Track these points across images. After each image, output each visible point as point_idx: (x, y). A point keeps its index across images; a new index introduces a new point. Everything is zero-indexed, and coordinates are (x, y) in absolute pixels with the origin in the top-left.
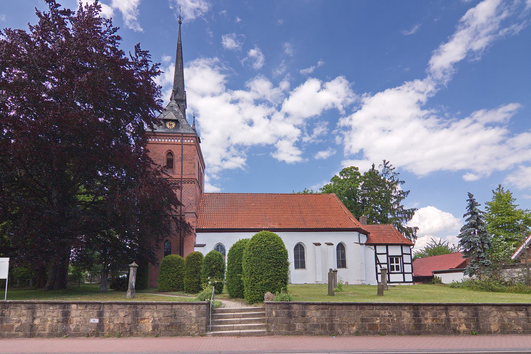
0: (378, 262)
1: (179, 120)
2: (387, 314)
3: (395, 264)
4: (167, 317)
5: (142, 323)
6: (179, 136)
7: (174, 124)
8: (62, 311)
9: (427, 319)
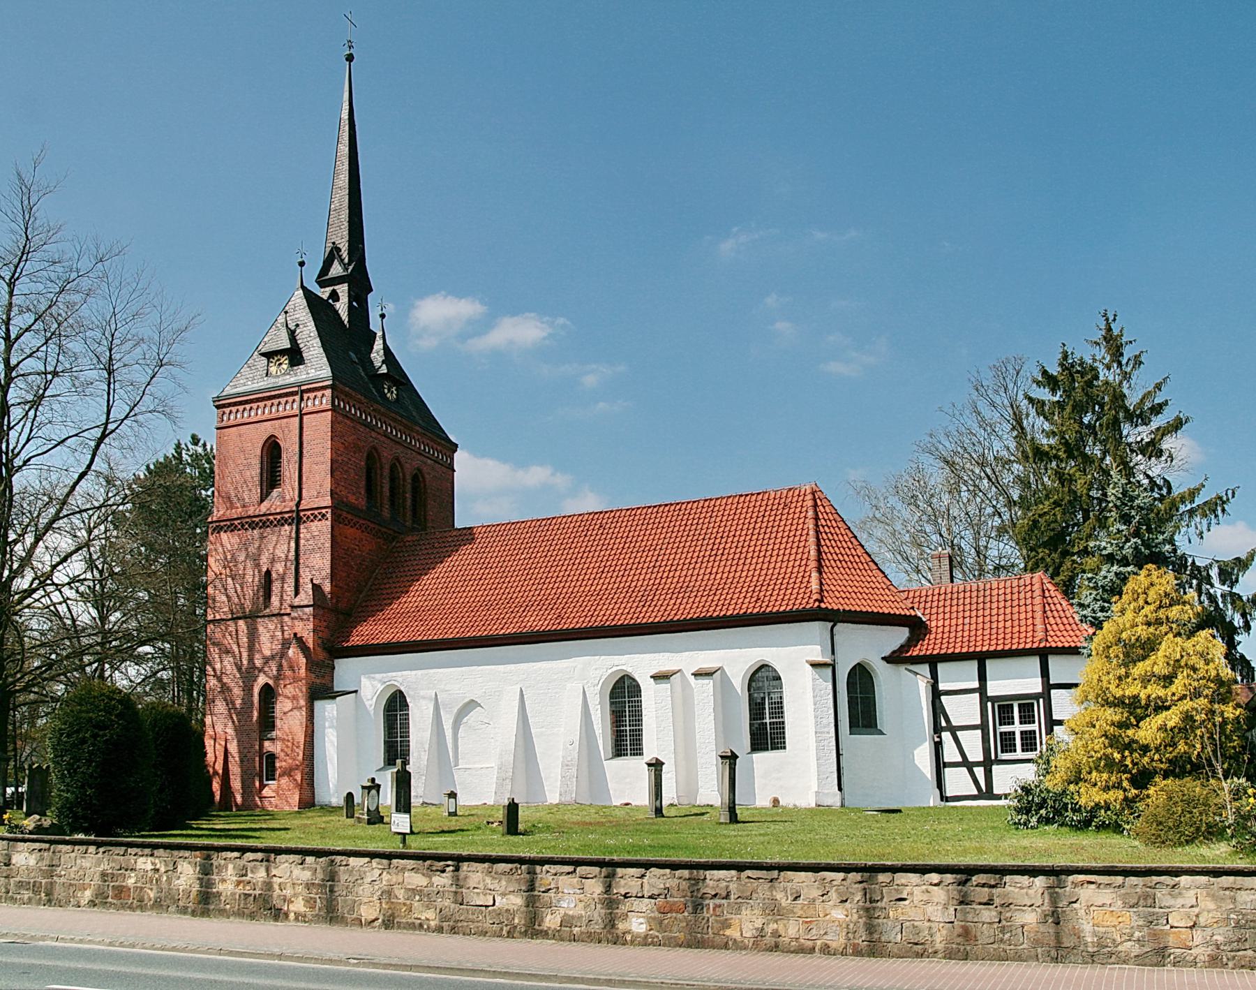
0: (944, 724)
2: (149, 867)
3: (1017, 728)
9: (224, 881)
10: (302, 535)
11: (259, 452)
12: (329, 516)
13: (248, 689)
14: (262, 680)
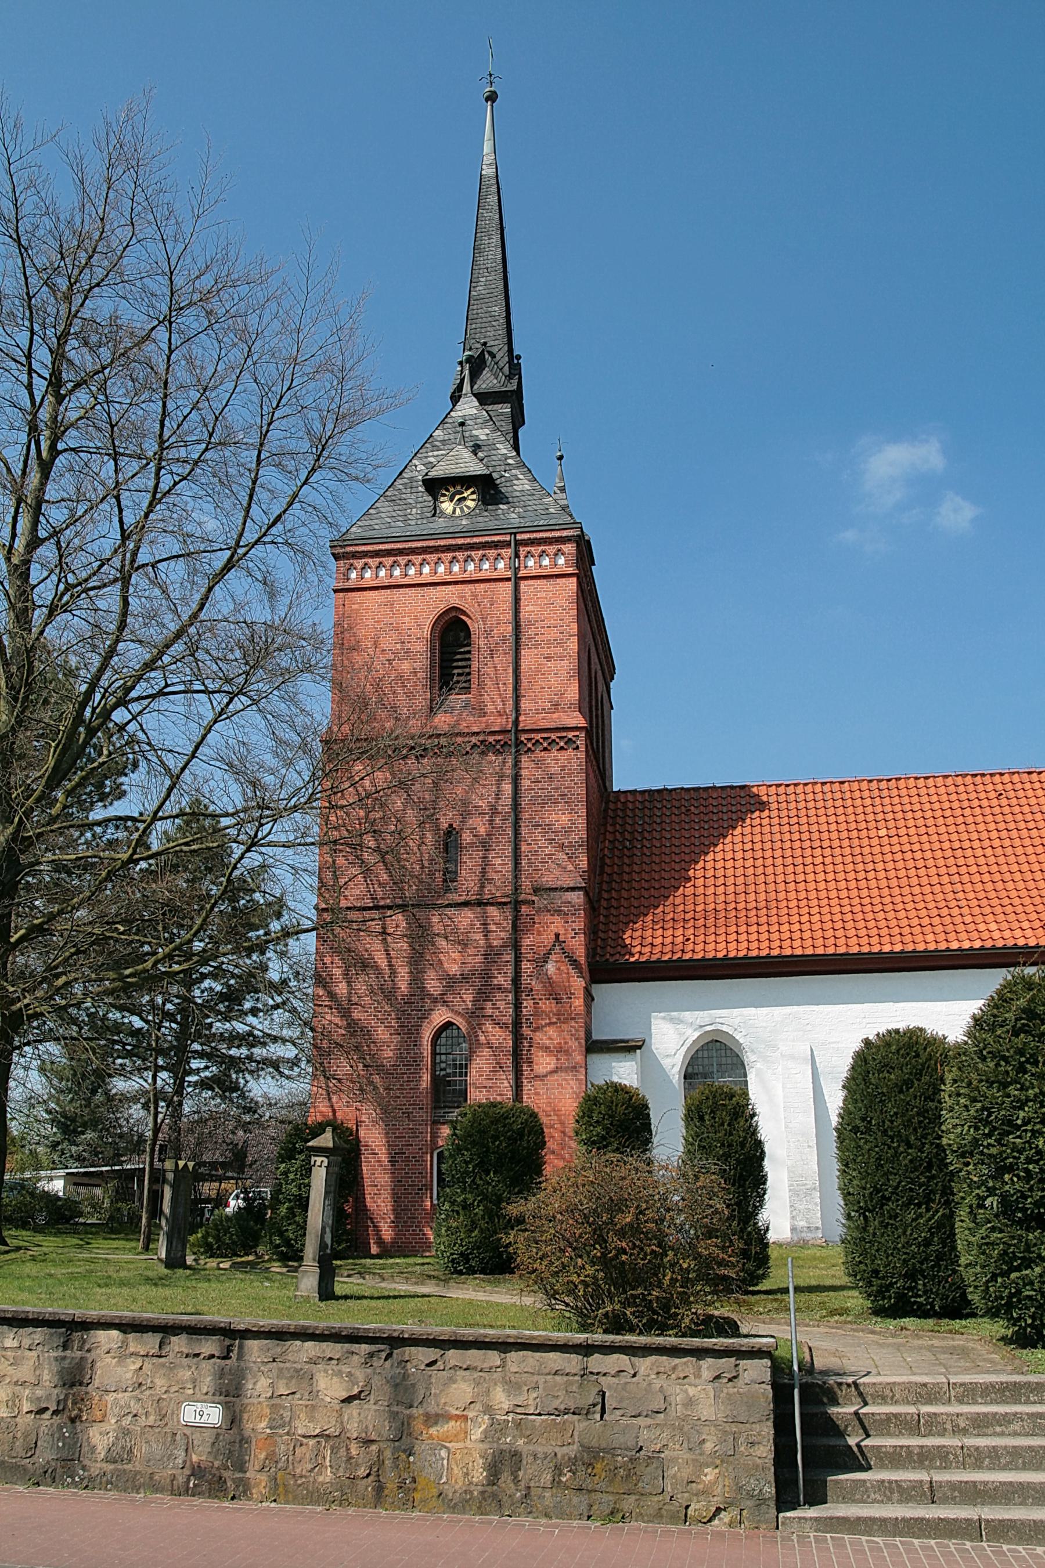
1: (495, 475)
4: (558, 1412)
5: (431, 1437)
6: (496, 545)
7: (474, 497)
8: (56, 1359)
10: (524, 773)
11: (427, 631)
12: (581, 743)
13: (409, 1032)
14: (440, 1016)
